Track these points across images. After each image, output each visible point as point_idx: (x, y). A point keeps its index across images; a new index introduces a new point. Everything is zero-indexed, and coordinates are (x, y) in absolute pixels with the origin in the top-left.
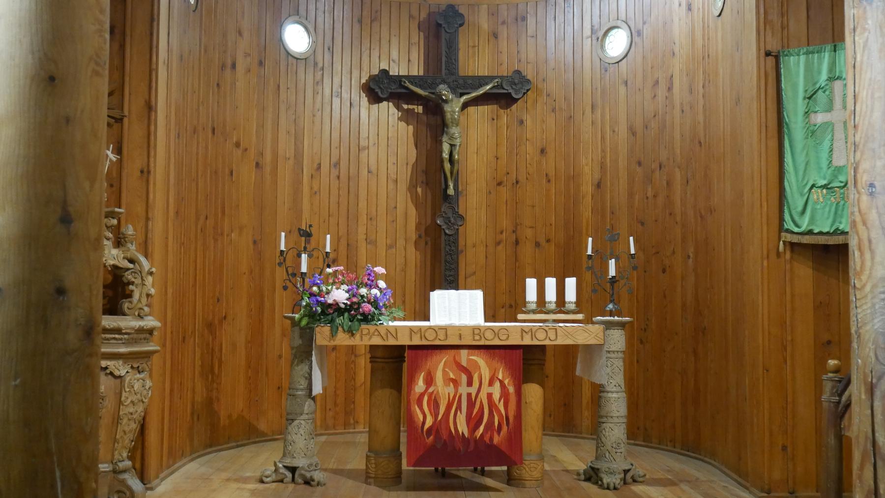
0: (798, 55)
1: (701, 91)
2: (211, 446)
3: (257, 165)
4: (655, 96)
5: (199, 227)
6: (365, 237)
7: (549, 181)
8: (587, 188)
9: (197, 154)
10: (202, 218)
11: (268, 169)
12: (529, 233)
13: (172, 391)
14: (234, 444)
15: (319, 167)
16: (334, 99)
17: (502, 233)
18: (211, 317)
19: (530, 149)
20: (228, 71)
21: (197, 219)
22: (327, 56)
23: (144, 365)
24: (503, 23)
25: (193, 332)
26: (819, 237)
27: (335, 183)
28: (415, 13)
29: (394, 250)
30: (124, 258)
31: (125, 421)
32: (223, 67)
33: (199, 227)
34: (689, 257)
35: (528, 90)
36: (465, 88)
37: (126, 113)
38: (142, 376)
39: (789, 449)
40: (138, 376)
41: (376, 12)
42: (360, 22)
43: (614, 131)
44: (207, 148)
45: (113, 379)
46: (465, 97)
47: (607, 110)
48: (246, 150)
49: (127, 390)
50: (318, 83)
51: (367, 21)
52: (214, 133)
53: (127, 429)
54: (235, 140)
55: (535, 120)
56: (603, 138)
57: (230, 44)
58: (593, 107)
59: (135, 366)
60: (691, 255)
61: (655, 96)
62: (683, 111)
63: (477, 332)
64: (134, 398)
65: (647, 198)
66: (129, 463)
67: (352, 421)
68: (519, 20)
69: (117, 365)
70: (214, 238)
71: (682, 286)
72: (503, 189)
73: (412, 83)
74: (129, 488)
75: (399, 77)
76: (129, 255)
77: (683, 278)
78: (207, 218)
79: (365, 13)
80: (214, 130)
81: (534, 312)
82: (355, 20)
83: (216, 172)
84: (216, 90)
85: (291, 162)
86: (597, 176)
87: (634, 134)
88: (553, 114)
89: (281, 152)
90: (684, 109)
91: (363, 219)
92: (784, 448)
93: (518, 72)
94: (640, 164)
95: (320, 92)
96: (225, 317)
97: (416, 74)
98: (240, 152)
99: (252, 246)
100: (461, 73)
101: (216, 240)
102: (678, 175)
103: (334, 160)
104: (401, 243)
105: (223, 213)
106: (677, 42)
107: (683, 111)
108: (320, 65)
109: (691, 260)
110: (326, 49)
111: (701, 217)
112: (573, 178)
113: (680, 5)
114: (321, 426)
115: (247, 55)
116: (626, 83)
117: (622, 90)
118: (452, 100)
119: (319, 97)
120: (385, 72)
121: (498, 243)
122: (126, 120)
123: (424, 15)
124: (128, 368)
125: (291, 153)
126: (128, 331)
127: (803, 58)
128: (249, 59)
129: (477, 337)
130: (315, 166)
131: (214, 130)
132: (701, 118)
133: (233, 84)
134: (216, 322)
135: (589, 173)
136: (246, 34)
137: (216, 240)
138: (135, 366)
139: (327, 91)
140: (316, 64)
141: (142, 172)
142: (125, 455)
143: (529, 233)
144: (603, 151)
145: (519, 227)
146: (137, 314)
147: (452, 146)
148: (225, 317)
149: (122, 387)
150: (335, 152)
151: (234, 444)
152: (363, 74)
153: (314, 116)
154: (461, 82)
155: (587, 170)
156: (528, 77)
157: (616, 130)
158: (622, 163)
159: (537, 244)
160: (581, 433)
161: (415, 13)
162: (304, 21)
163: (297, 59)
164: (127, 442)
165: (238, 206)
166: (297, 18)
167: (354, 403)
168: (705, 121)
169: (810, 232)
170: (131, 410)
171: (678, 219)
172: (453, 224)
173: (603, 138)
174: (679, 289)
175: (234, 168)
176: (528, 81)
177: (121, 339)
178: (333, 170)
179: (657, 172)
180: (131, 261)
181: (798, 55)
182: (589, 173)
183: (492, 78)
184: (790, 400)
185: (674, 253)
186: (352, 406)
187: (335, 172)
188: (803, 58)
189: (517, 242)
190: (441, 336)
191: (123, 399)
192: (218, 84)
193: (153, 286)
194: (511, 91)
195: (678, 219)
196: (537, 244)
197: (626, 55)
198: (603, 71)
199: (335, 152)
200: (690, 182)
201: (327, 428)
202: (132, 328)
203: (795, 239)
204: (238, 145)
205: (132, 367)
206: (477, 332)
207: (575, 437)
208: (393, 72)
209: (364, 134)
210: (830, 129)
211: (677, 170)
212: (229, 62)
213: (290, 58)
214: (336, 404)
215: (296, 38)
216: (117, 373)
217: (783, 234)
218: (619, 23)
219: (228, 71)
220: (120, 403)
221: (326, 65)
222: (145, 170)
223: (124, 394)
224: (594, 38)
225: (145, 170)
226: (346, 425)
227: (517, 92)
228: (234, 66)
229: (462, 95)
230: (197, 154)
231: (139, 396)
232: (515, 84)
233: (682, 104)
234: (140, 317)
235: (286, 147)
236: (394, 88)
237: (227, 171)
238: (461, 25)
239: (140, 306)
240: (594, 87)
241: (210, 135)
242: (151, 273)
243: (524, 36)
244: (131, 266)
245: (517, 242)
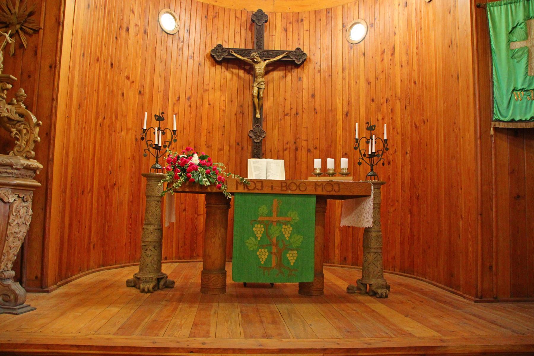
0: (500, 5)
1: (415, 51)
2: (103, 266)
3: (140, 92)
4: (383, 60)
5: (98, 124)
6: (205, 143)
7: (316, 113)
8: (340, 116)
9: (99, 75)
10: (100, 119)
11: (147, 96)
12: (304, 143)
13: (70, 225)
14: (119, 265)
15: (178, 100)
16: (189, 60)
17: (287, 143)
18: (105, 183)
19: (305, 93)
20: (124, 32)
21: (97, 118)
22: (186, 35)
23: (28, 196)
24: (290, 23)
25: (91, 190)
26: (519, 124)
27: (188, 110)
28: (239, 15)
29: (222, 152)
30: (16, 113)
31: (11, 239)
32: (120, 28)
33: (98, 124)
34: (407, 153)
35: (305, 60)
36: (267, 57)
37: (42, 26)
38: (26, 204)
39: (494, 269)
40: (24, 204)
41: (216, 13)
42: (206, 17)
43: (356, 83)
44: (106, 74)
45: (3, 204)
46: (268, 61)
47: (352, 70)
48: (133, 82)
49: (14, 214)
50: (180, 49)
51: (210, 17)
52: (112, 67)
53: (12, 245)
54: (126, 74)
55: (307, 78)
56: (350, 87)
57: (125, 16)
58: (343, 69)
59: (21, 196)
60: (408, 152)
61: (383, 60)
62: (402, 66)
63: (284, 184)
64: (20, 221)
65: (378, 120)
66: (13, 273)
67: (195, 255)
68: (299, 21)
69: (6, 194)
70: (109, 132)
71: (402, 171)
72: (288, 118)
73: (235, 52)
74: (13, 292)
75: (229, 49)
76: (20, 111)
77: (402, 166)
78: (104, 118)
79: (209, 13)
80: (112, 64)
81: (319, 175)
82: (204, 16)
83: (112, 91)
84: (115, 40)
85: (161, 94)
86: (346, 109)
87: (369, 83)
88: (319, 74)
89: (155, 87)
90: (403, 64)
91: (204, 132)
92: (491, 267)
93: (298, 49)
94: (373, 100)
95: (181, 55)
96: (115, 184)
97: (238, 48)
98: (129, 83)
99: (134, 143)
100: (265, 48)
101: (110, 134)
102: (399, 105)
103: (188, 96)
104: (226, 148)
105: (116, 118)
106: (397, 27)
107: (402, 66)
108: (182, 39)
109: (408, 155)
110: (186, 31)
111: (416, 127)
112: (332, 111)
113: (399, 5)
114: (176, 257)
115: (136, 25)
116: (364, 54)
117: (362, 59)
118: (260, 62)
119: (180, 58)
120: (220, 46)
121: (286, 150)
122: (41, 31)
123: (244, 18)
124: (15, 197)
125: (161, 89)
126: (18, 167)
127: (503, 7)
128: (137, 28)
129: (284, 188)
130: (176, 98)
131: (112, 64)
132: (415, 67)
133: (127, 40)
134: (109, 187)
135: (340, 108)
136: (136, 13)
137: (110, 134)
138: (21, 196)
139: (185, 55)
140: (179, 38)
141: (51, 67)
142: (10, 265)
143: (304, 143)
144: (350, 94)
145: (298, 140)
146: (24, 155)
147: (259, 89)
148: (115, 184)
149: (10, 211)
150: (189, 91)
151: (119, 265)
152: (207, 47)
153: (177, 68)
154: (265, 53)
155: (340, 106)
156: (304, 52)
157: (358, 82)
158: (362, 101)
159: (309, 150)
160: (334, 263)
161: (239, 15)
162: (173, 13)
163: (168, 34)
164: (11, 255)
165: (126, 115)
166: (168, 10)
167: (196, 243)
168: (418, 68)
169: (513, 121)
170: (17, 230)
171: (399, 131)
172: (259, 136)
173: (350, 87)
174: (399, 173)
175: (125, 91)
176: (305, 54)
177: (12, 173)
178: (187, 101)
179: (385, 104)
180: (21, 115)
181: (500, 5)
182: (340, 108)
183: (283, 52)
184: (494, 234)
185: (396, 151)
186: (195, 245)
187: (188, 103)
188: (503, 7)
189: (296, 149)
190: (259, 186)
191: (10, 220)
192: (116, 38)
193: (39, 135)
194: (295, 60)
195: (399, 131)
196: (309, 150)
197: (364, 38)
198: (350, 48)
199: (189, 91)
200: (407, 108)
201: (180, 258)
202: (22, 165)
203: (502, 126)
204: (128, 78)
205: (19, 197)
206: (284, 184)
207: (331, 266)
208: (225, 46)
209: (206, 82)
210: (526, 52)
211: (398, 101)
212: (125, 26)
213: (163, 32)
214: (185, 244)
215: (168, 22)
216: (6, 200)
217: (493, 123)
218: (359, 20)
219: (124, 32)
220: (8, 223)
221: (185, 40)
222: (54, 66)
223: (12, 217)
224: (344, 30)
225: (54, 66)
226: (191, 257)
227: (299, 60)
228: (128, 29)
229: (265, 60)
230: (99, 75)
231: (23, 219)
232: (297, 56)
233: (401, 62)
234: (27, 158)
235: (159, 84)
236: (225, 55)
237: (120, 93)
238: (266, 22)
239: (28, 149)
240: (344, 58)
241: (109, 67)
242: (38, 125)
243: (302, 30)
244: (22, 119)
245: (296, 149)
